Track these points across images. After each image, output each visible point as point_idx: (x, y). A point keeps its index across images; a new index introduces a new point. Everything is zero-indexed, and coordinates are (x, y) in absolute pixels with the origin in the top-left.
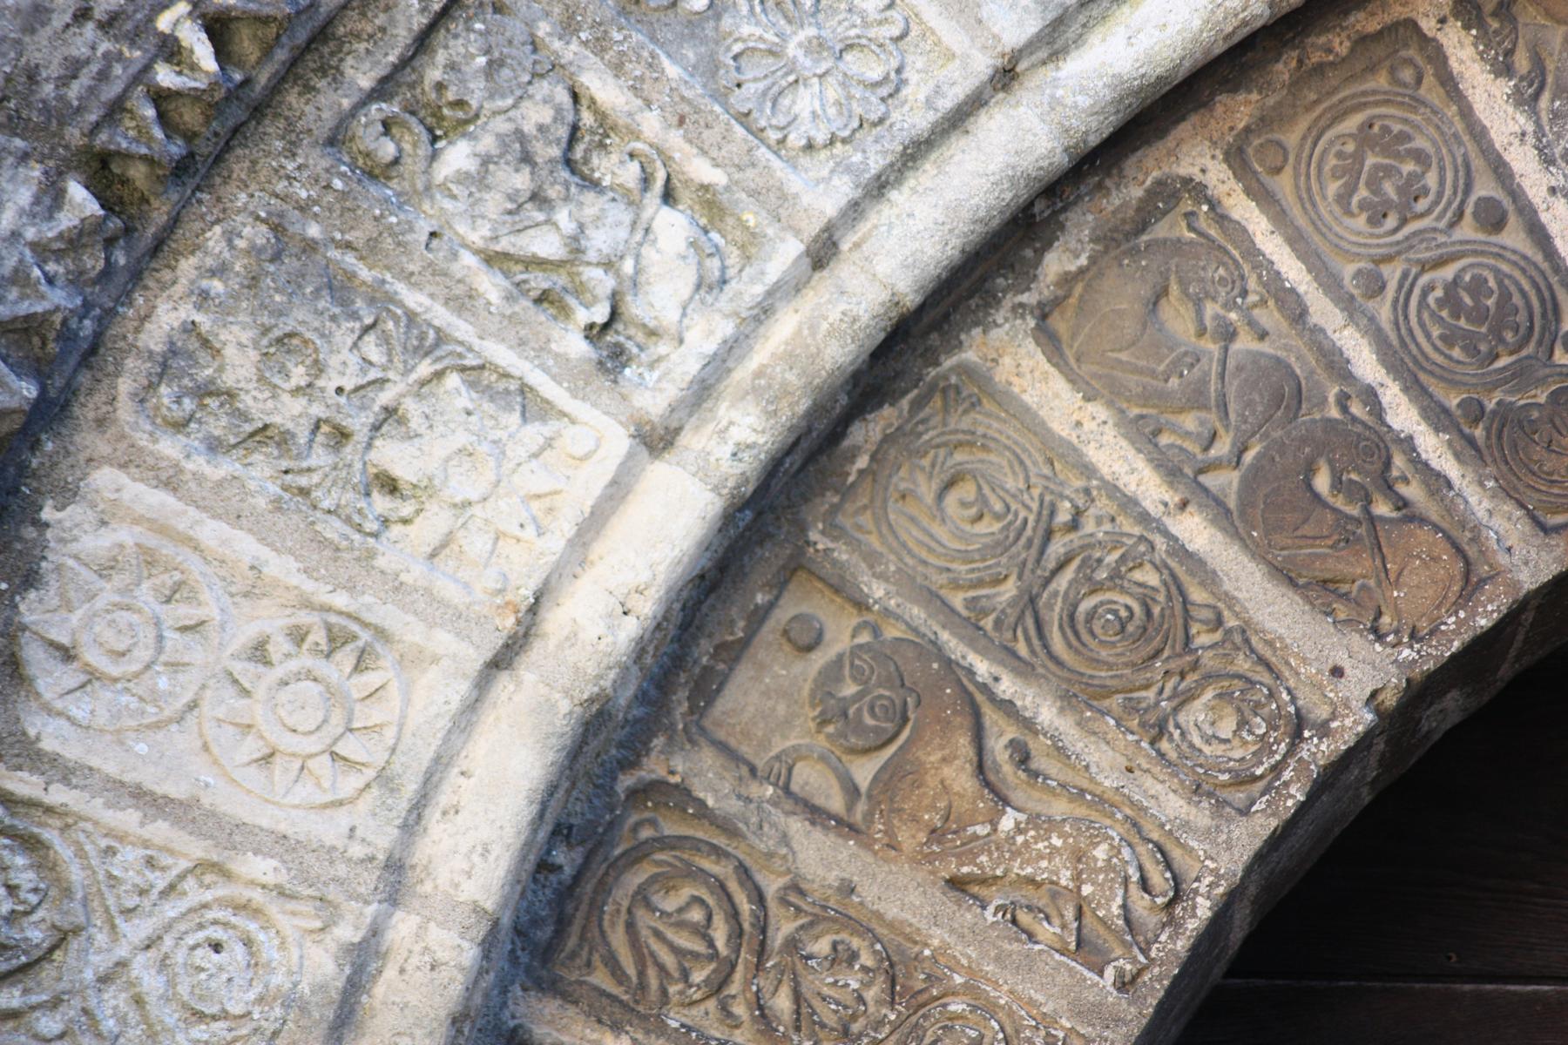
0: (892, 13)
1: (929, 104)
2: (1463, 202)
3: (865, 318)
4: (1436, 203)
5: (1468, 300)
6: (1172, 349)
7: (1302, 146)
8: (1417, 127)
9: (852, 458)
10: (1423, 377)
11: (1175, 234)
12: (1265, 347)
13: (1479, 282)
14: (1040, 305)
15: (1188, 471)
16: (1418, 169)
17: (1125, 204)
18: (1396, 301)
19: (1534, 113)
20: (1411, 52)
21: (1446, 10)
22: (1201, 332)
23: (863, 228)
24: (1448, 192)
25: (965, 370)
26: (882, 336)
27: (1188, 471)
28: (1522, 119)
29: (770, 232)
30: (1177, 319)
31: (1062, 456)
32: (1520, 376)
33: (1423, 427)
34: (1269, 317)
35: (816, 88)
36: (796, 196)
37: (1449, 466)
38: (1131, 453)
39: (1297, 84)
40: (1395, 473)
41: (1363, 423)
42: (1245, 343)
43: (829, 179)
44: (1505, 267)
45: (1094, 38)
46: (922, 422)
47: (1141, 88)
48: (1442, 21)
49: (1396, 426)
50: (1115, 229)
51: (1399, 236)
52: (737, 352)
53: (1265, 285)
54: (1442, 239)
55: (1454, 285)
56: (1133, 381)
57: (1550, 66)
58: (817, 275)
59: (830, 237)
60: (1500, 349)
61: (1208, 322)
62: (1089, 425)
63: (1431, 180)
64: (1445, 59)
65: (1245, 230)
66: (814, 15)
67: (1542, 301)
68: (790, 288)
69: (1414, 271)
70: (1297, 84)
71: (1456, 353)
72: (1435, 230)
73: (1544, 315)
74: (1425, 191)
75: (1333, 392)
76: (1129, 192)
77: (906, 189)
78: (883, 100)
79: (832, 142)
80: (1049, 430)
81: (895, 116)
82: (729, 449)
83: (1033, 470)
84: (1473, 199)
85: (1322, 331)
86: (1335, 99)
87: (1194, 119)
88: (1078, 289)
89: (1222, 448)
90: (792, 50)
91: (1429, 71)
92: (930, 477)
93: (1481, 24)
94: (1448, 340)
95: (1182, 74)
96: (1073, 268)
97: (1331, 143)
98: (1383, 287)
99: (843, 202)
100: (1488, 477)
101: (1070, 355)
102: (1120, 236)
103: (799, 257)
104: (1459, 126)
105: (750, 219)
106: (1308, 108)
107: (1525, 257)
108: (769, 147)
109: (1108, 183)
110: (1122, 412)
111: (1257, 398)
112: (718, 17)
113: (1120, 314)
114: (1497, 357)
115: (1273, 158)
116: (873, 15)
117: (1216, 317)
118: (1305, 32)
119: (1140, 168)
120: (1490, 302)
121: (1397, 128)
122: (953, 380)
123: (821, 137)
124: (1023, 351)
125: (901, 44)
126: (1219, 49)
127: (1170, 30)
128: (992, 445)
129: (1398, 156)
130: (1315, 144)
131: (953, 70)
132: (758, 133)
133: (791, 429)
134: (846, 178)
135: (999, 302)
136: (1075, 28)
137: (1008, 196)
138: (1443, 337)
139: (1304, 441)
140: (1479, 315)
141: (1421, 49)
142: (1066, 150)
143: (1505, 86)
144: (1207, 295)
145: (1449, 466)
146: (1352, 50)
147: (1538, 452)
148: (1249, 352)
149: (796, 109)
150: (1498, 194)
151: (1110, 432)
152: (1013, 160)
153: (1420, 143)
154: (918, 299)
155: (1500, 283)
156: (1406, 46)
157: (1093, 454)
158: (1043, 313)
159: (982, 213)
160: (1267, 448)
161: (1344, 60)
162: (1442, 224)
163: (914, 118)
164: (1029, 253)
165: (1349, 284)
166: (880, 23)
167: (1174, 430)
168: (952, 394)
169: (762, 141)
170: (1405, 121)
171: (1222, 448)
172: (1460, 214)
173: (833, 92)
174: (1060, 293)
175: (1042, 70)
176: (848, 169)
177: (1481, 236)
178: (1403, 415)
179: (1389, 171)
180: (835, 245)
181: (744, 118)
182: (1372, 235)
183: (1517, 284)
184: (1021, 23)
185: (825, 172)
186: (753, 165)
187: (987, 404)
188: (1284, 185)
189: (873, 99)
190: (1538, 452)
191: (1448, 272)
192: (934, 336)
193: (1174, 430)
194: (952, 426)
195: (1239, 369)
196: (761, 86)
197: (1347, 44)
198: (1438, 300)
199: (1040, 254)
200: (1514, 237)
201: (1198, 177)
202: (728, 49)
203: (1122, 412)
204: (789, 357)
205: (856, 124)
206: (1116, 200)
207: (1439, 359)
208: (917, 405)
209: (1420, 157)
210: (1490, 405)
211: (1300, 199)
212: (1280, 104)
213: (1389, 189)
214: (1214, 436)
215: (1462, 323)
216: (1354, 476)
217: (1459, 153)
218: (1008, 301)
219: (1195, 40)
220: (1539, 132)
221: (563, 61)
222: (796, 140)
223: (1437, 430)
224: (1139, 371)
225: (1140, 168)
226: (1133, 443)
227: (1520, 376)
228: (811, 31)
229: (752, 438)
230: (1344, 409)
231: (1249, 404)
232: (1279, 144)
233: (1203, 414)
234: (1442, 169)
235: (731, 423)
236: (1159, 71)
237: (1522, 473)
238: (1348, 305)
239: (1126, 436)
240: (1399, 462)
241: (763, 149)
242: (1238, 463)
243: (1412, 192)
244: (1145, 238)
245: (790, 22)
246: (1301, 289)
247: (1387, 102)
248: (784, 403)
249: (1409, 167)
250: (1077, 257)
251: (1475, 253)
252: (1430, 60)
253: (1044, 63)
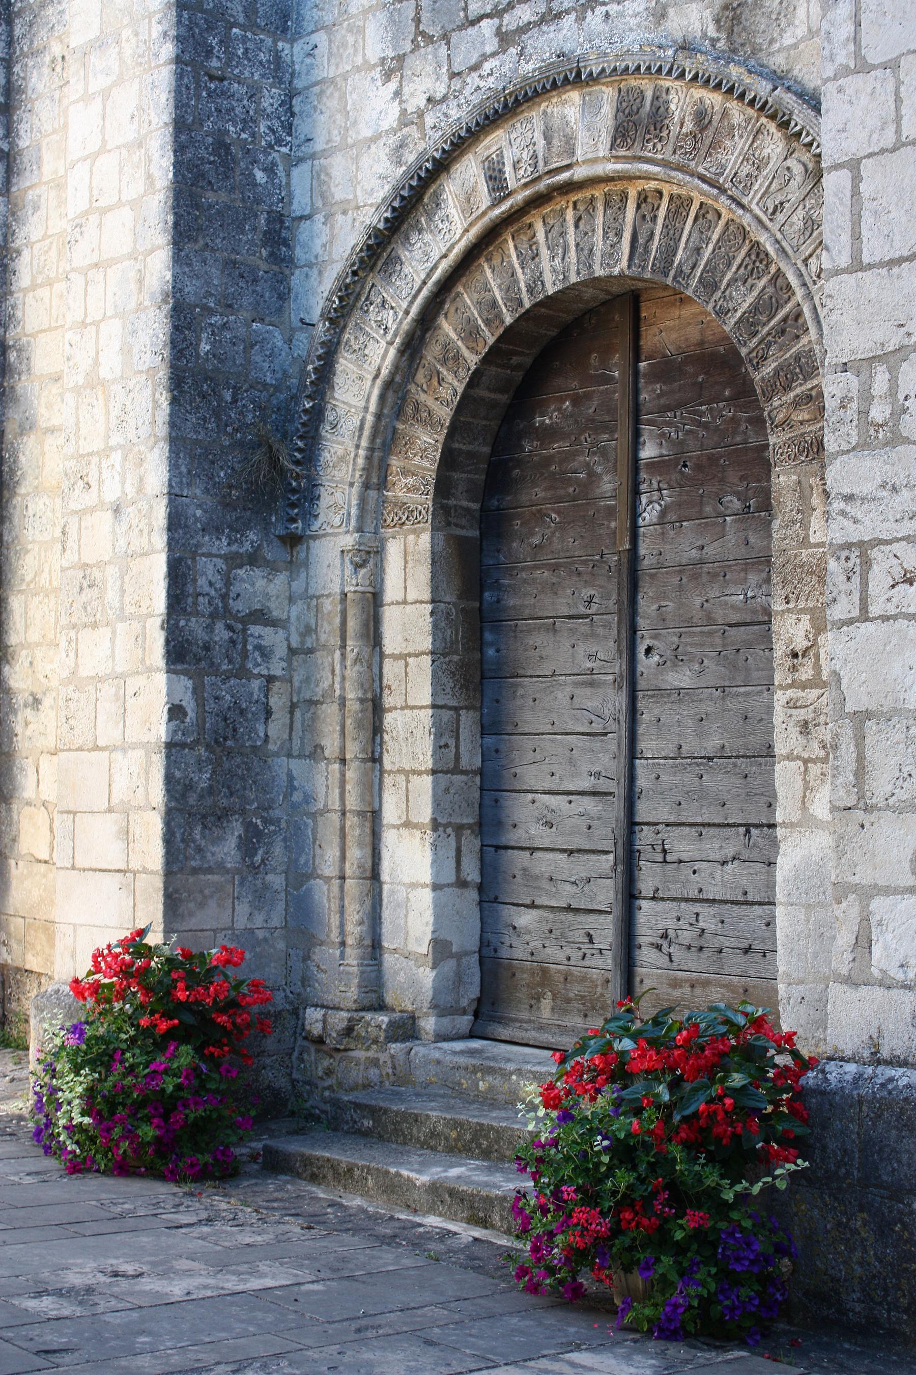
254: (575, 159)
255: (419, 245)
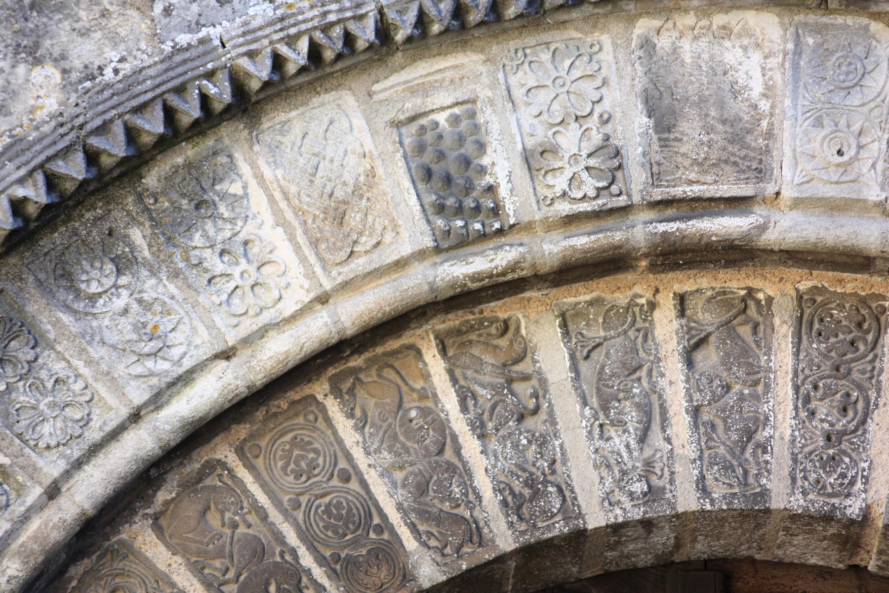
0: (86, 391)
1: (101, 429)
2: (333, 470)
3: (69, 520)
4: (322, 470)
5: (334, 511)
6: (210, 532)
7: (267, 446)
8: (315, 439)
9: (70, 581)
10: (315, 544)
11: (214, 483)
12: (250, 531)
13: (339, 504)
14: (155, 514)
15: (216, 585)
16: (315, 456)
17: (192, 471)
18: (305, 511)
19: (363, 434)
20: (313, 408)
21: (327, 391)
22: (223, 525)
23: (72, 482)
24: (327, 466)
25: (121, 542)
26: (78, 528)
27: (216, 585)
28: (357, 436)
29: (29, 484)
30: (214, 520)
31: (162, 579)
32: (355, 543)
33: (315, 565)
34: (252, 518)
35: (52, 423)
36: (41, 468)
37: (325, 581)
38: (191, 577)
39: (266, 420)
40: (303, 585)
41: (290, 563)
42: (242, 529)
43: (55, 462)
44: (350, 497)
45: (174, 401)
46: (102, 565)
47: (193, 422)
48: (326, 395)
49: (304, 565)
50: (188, 482)
51: (307, 484)
52: (13, 536)
53: (250, 505)
54: (324, 485)
55: (328, 506)
56: (193, 546)
57: (369, 414)
58: (51, 502)
59: (56, 486)
60: (347, 532)
61: (226, 521)
62: (174, 566)
63: (321, 461)
64: (327, 411)
65: (242, 482)
66: (52, 392)
67: (365, 511)
68: (37, 508)
69: (313, 499)
70: (266, 420)
71: (330, 533)
72: (321, 482)
73: (365, 518)
74: (318, 465)
75: (278, 550)
76: (194, 466)
77: (91, 465)
78: (81, 427)
79: (58, 445)
80: (157, 568)
81: (86, 434)
82: (5, 579)
83: (149, 585)
84: (337, 469)
85: (274, 524)
86: (282, 427)
87: (223, 435)
88: (172, 507)
89: (231, 575)
90: (42, 407)
91: (320, 416)
92: (104, 589)
93: (341, 397)
94: (326, 528)
95: (211, 417)
96: (169, 498)
97: (280, 445)
98: (300, 506)
99: (62, 470)
100: (341, 586)
101: (167, 535)
102: (189, 484)
103: (41, 495)
104: (332, 439)
105: (20, 479)
106: (271, 430)
107: (358, 493)
108: (30, 448)
109: (185, 462)
110: (188, 559)
111: (245, 552)
112: (10, 393)
113: (189, 517)
114: (346, 535)
115: (255, 451)
116: (78, 392)
117: (230, 518)
118: (269, 398)
119: (199, 456)
120: (344, 512)
121: (306, 439)
122: (116, 547)
123: (53, 443)
124: (146, 534)
125: (90, 404)
126: (227, 406)
127: (206, 398)
128: (132, 574)
129: (306, 451)
130: (273, 445)
131: (112, 414)
132: (26, 442)
133: (35, 569)
134: (63, 461)
135: (137, 513)
136: (166, 397)
137: (134, 467)
138: (324, 527)
139: (265, 571)
140: (339, 518)
141: (317, 407)
142: (160, 448)
143: (351, 422)
144: (226, 509)
145: (325, 581)
146: (289, 407)
147: (361, 575)
148: (243, 533)
149: (43, 432)
150: (347, 467)
151: (183, 568)
152: (137, 452)
153: (316, 445)
154: (94, 512)
155: (348, 504)
156: (311, 405)
157: (175, 578)
158: (156, 517)
159: (122, 475)
160: (249, 575)
161: (285, 411)
162: (325, 479)
163: (94, 435)
164: (150, 492)
165: (286, 504)
166: (81, 395)
167: (210, 567)
168: (115, 553)
169: (28, 445)
170: (310, 436)
171: (231, 575)
172: (332, 475)
173: (59, 424)
174: (164, 509)
175: (152, 415)
176: (64, 457)
177: (341, 485)
178: (307, 560)
179: (303, 457)
180: (59, 489)
181: (19, 436)
182: (296, 484)
183: (355, 504)
184: (141, 395)
185: (55, 458)
186: (23, 455)
187: (131, 557)
188: (260, 463)
189: (77, 427)
190: (361, 575)
191: (327, 500)
192: (108, 528)
193: (210, 567)
194: (115, 567)
195: (239, 540)
196: (28, 422)
197: (287, 404)
198: (322, 511)
199: (155, 492)
200: (354, 485)
201: (224, 459)
202: (14, 407)
203: (188, 559)
204: (35, 538)
205: (68, 437)
206: (188, 469)
207: (322, 536)
208: (100, 558)
209: (316, 451)
210: (343, 556)
211: (266, 468)
212: (258, 429)
213: (303, 464)
214: (227, 570)
215: (332, 521)
216: (285, 586)
217: (332, 449)
218: (141, 513)
219: (215, 402)
220: (365, 441)
221: (360, 393)
222: (42, 444)
223: (320, 566)
224: (196, 542)
225: (199, 456)
226: (192, 572)
227: (355, 543)
228: (51, 399)
229: (16, 574)
230: (282, 557)
231: (243, 555)
232: (258, 446)
233: (223, 560)
234: (325, 456)
235: (8, 567)
236: (200, 415)
237: (355, 584)
238: (285, 513)
239: (189, 570)
240: (305, 580)
241: (27, 449)
242: (237, 581)
243: (313, 466)
244: (201, 485)
245: (42, 395)
246: (266, 506)
247: (302, 429)
248: (32, 558)
249: (311, 455)
250: (171, 493)
251: (338, 491)
252: (320, 411)
253: (153, 411)
254: (770, 189)
255: (119, 303)
